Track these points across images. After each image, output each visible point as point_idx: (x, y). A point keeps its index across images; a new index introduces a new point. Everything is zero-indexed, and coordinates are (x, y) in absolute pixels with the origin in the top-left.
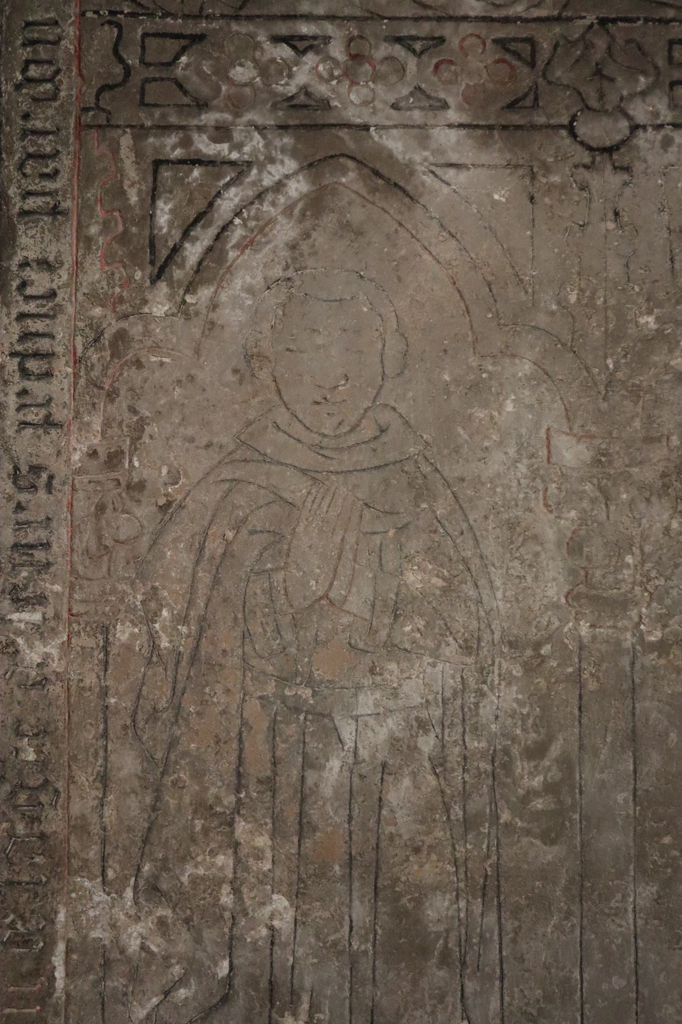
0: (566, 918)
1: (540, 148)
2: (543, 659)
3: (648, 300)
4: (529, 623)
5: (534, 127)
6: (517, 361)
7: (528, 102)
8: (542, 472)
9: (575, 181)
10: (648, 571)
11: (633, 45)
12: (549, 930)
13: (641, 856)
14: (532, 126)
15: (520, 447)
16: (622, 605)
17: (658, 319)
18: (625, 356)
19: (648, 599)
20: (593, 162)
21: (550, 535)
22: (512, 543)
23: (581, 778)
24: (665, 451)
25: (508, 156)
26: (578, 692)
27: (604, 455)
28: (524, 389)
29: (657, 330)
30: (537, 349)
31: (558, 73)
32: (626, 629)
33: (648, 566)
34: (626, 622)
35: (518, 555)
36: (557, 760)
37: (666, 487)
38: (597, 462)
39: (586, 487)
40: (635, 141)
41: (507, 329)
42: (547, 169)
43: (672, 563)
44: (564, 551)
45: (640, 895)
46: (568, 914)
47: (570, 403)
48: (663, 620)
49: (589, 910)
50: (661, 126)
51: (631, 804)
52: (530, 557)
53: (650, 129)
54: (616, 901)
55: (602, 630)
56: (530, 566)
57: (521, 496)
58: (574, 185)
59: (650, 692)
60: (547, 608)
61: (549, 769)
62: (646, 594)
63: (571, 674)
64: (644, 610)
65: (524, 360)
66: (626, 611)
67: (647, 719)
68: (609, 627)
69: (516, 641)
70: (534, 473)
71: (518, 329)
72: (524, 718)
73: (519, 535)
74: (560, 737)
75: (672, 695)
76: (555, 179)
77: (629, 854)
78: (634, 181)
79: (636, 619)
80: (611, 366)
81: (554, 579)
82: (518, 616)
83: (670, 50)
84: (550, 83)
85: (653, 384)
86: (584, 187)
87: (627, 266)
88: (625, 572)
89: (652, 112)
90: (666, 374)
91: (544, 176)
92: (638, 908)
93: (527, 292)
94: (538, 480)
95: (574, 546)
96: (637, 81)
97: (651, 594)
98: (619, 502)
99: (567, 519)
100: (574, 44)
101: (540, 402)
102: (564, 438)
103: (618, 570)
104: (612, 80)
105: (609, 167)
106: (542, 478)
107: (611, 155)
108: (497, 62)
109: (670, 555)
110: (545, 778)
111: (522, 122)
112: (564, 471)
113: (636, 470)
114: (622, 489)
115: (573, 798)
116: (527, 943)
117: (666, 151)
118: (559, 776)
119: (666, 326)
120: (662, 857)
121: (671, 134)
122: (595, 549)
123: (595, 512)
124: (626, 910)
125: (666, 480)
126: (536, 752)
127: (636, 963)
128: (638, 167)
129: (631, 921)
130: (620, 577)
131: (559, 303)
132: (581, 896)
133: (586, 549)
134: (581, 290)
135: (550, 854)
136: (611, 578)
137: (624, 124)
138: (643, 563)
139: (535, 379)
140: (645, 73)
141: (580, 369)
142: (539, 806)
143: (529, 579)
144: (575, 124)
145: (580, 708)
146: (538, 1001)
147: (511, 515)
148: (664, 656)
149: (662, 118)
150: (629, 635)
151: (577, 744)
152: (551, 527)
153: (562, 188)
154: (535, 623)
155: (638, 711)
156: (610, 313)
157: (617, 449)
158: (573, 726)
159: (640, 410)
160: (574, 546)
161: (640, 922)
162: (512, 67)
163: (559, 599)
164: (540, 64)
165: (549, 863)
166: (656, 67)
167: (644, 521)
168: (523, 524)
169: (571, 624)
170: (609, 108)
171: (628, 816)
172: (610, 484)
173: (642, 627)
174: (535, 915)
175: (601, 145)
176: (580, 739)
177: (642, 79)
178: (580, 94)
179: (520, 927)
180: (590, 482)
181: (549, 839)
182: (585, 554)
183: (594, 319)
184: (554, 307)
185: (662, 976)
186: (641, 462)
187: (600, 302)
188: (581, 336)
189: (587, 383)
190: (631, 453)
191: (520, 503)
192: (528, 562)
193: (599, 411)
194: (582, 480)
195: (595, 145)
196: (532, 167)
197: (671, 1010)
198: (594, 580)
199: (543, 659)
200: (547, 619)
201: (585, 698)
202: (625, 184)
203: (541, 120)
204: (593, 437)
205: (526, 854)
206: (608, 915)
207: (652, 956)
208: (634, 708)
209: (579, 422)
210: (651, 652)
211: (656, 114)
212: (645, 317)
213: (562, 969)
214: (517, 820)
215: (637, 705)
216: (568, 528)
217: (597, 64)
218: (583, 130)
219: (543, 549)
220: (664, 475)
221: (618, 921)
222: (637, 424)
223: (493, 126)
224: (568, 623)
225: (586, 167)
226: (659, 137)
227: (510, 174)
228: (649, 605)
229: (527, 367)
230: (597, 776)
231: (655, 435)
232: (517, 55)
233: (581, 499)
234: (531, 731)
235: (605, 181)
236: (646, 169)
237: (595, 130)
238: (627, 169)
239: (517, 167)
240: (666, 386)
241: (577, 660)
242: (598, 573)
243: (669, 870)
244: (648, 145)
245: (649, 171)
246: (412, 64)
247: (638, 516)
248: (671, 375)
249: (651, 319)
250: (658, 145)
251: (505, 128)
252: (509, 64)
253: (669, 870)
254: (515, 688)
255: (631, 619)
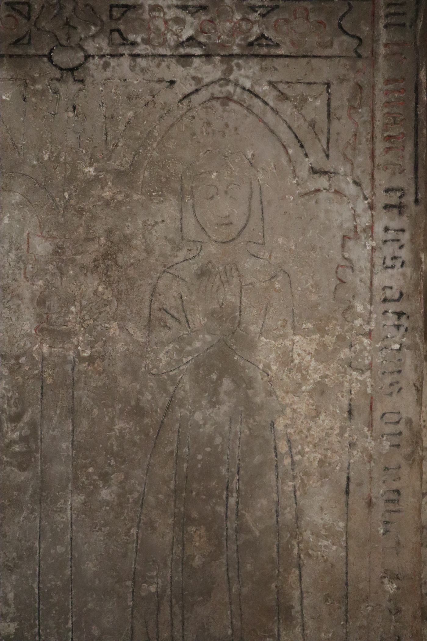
0: (31, 513)
1: (30, 69)
2: (20, 365)
3: (91, 158)
4: (13, 345)
5: (28, 56)
6: (12, 194)
7: (25, 41)
8: (23, 258)
9: (51, 88)
10: (84, 315)
11: (88, 7)
12: (21, 519)
13: (76, 478)
14: (27, 55)
15: (11, 243)
16: (68, 335)
17: (96, 169)
18: (76, 191)
19: (83, 332)
20: (62, 77)
21: (27, 294)
22: (4, 298)
23: (41, 434)
24: (97, 246)
25: (12, 73)
26: (41, 385)
27: (60, 248)
28: (15, 210)
29: (94, 176)
30: (24, 187)
31: (43, 24)
32: (70, 349)
33: (84, 312)
34: (70, 345)
35: (7, 305)
36: (27, 423)
37: (96, 267)
38: (55, 252)
39: (49, 267)
40: (87, 64)
41: (7, 175)
42: (34, 81)
43: (98, 311)
44: (35, 304)
45: (74, 500)
46: (32, 511)
47: (41, 218)
48: (91, 344)
49: (44, 509)
50: (104, 56)
51: (70, 449)
52: (15, 307)
53: (97, 58)
54: (61, 504)
55: (55, 349)
56: (15, 312)
57: (11, 272)
58: (50, 91)
59: (82, 385)
60: (23, 336)
61: (22, 428)
62: (82, 329)
63: (37, 374)
64: (81, 338)
65: (16, 193)
66: (70, 339)
67: (81, 401)
68: (60, 348)
69: (5, 355)
70: (19, 259)
71: (13, 175)
72: (9, 399)
73: (9, 294)
74: (30, 410)
75: (96, 387)
76: (39, 87)
77: (68, 478)
78: (86, 87)
79: (76, 343)
80: (67, 197)
81: (28, 320)
82: (7, 341)
83: (111, 11)
84: (39, 29)
85: (91, 207)
86: (56, 92)
87: (79, 138)
88: (70, 316)
89: (98, 48)
90: (99, 201)
91: (32, 85)
92: (73, 508)
93: (19, 154)
94: (21, 263)
95: (41, 302)
96: (90, 29)
97: (85, 329)
98: (68, 275)
99: (37, 285)
100: (54, 6)
101: (24, 218)
102: (38, 239)
103: (66, 315)
104: (75, 28)
105: (71, 79)
106: (23, 261)
107: (73, 73)
108: (8, 16)
109: (97, 306)
110: (21, 433)
111: (20, 53)
112: (37, 257)
113: (79, 257)
114: (70, 268)
115: (37, 445)
116: (8, 526)
117: (105, 70)
118: (29, 432)
119: (101, 173)
120: (87, 479)
121: (108, 60)
122: (53, 302)
123: (54, 281)
124: (66, 509)
125: (96, 263)
126: (16, 418)
127: (72, 539)
128: (89, 80)
129: (69, 515)
130: (67, 319)
131: (38, 160)
132: (40, 500)
133: (47, 303)
134: (52, 153)
135: (22, 476)
136: (61, 320)
137: (81, 54)
138: (81, 311)
139: (21, 205)
140: (95, 24)
141: (48, 198)
142: (17, 449)
143: (14, 319)
144: (52, 54)
145: (42, 394)
146: (14, 559)
147: (4, 283)
148: (92, 364)
149: (104, 51)
150: (71, 353)
151: (39, 414)
152: (28, 290)
153: (43, 92)
154: (16, 345)
155: (75, 396)
156: (67, 166)
157: (68, 245)
158: (37, 404)
159: (83, 223)
160: (41, 301)
161: (74, 516)
162: (16, 20)
163: (31, 331)
164: (33, 18)
165: (22, 482)
166: (102, 21)
167: (83, 287)
168: (11, 288)
169: (37, 346)
170: (73, 45)
171: (68, 456)
172: (63, 265)
173: (79, 348)
174: (13, 511)
175: (67, 67)
176: (42, 411)
177: (93, 28)
178: (56, 36)
179: (4, 518)
180: (52, 264)
181: (22, 467)
182: (47, 305)
183: (58, 169)
184: (35, 163)
185: (86, 546)
186: (82, 253)
187: (62, 159)
188: (50, 179)
189: (52, 206)
190: (76, 247)
191: (10, 276)
192: (13, 310)
193: (58, 222)
194: (47, 263)
195: (64, 67)
196: (26, 80)
197: (90, 565)
198: (52, 320)
199: (20, 365)
200: (24, 343)
201: (44, 388)
202: (80, 90)
203: (32, 51)
204: (54, 238)
205: (8, 476)
206: (56, 512)
207: (81, 535)
208: (73, 394)
209: (46, 229)
210: (84, 362)
211: (101, 49)
212: (88, 168)
213: (28, 542)
214: (4, 456)
215: (75, 393)
216: (37, 290)
217: (67, 19)
218: (56, 58)
219: (23, 303)
220: (95, 260)
221: (61, 515)
222: (81, 230)
223: (4, 55)
224: (36, 345)
225: (58, 80)
226: (102, 62)
227: (12, 84)
228: (84, 335)
229: (17, 197)
230: (51, 432)
231: (91, 236)
232: (20, 13)
233: (46, 274)
234: (13, 406)
235: (69, 88)
236: (93, 81)
237: (64, 58)
238: (82, 81)
239: (17, 79)
240: (99, 208)
241: (40, 366)
242: (54, 316)
243: (92, 487)
244: (95, 67)
245: (95, 82)
246: (189, 19)
247: (79, 284)
248: (102, 202)
249: (91, 169)
250: (100, 67)
251: (11, 56)
252: (15, 18)
253: (92, 487)
254: (4, 382)
255: (73, 343)
